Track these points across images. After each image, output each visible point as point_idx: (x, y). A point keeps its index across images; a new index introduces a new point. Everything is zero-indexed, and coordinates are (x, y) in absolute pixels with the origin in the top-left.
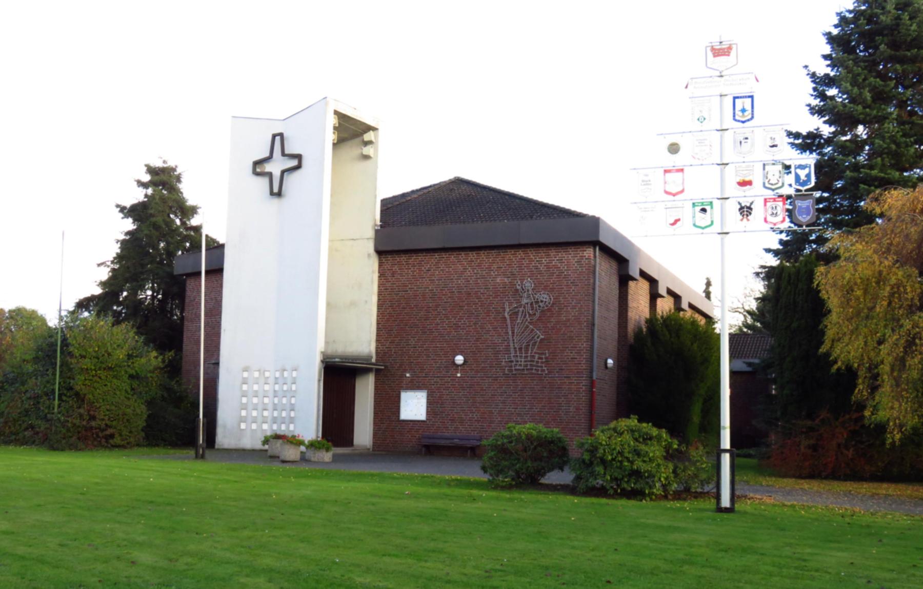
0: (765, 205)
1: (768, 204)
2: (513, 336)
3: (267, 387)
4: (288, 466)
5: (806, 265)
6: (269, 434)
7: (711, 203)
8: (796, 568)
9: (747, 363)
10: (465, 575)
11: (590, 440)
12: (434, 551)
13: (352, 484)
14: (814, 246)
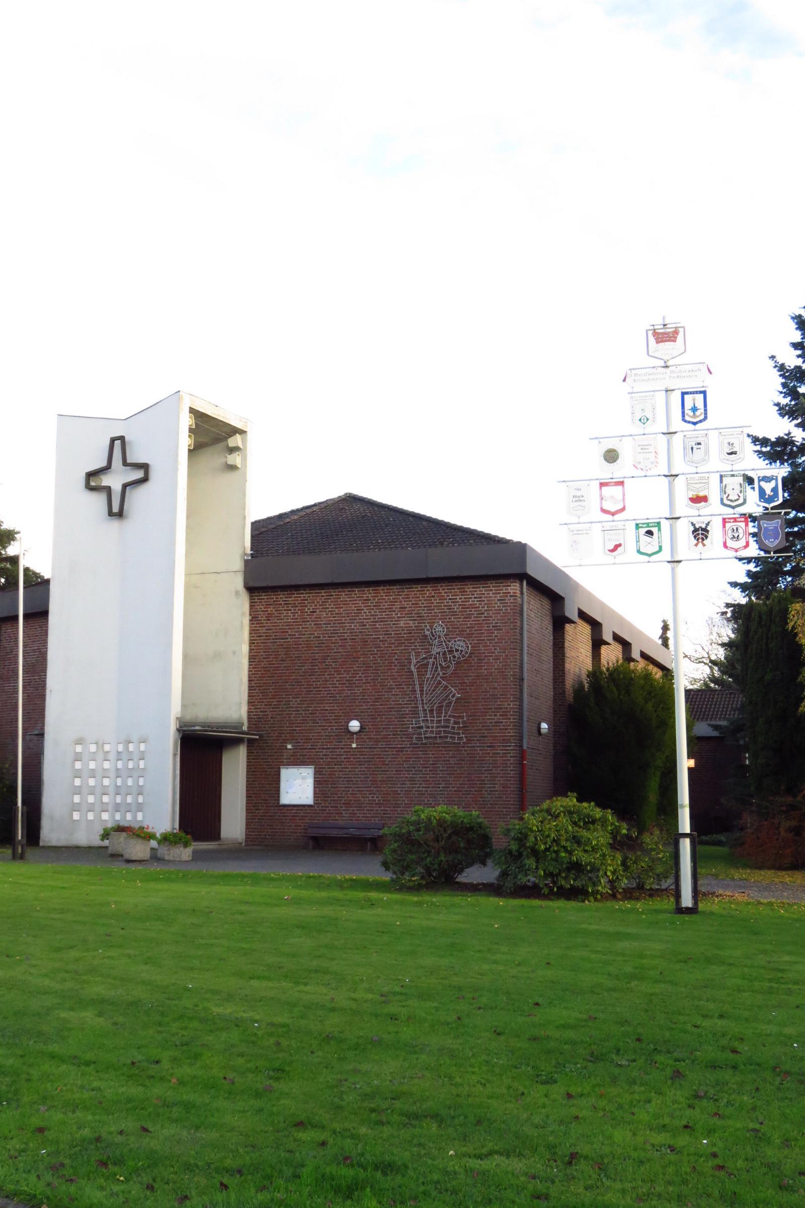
0: (724, 526)
1: (728, 525)
2: (422, 694)
3: (107, 765)
4: (133, 867)
5: (779, 602)
6: (110, 825)
7: (659, 523)
8: (770, 980)
9: (712, 726)
10: (355, 1000)
11: (516, 824)
12: (316, 971)
13: (216, 888)
14: (789, 579)
